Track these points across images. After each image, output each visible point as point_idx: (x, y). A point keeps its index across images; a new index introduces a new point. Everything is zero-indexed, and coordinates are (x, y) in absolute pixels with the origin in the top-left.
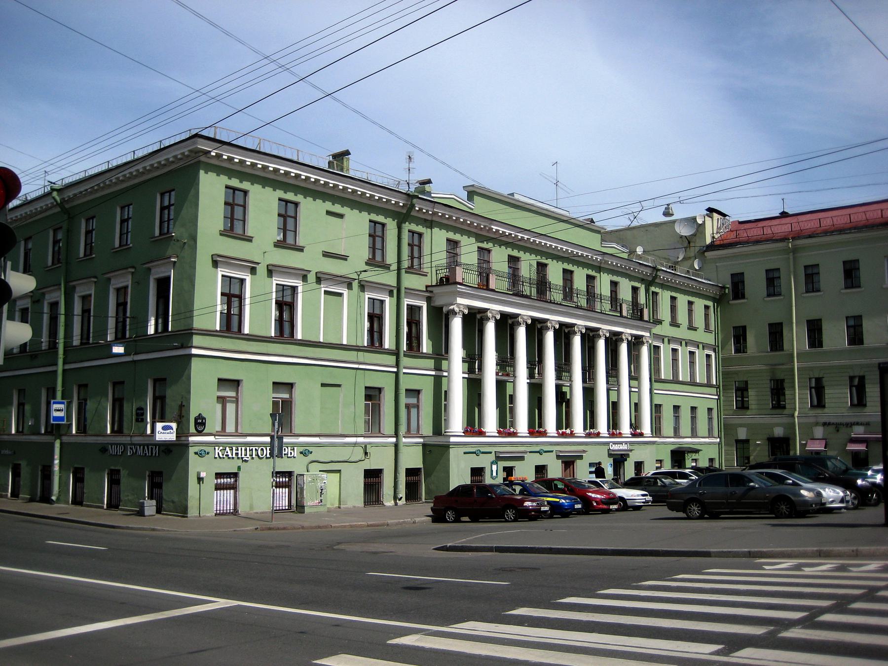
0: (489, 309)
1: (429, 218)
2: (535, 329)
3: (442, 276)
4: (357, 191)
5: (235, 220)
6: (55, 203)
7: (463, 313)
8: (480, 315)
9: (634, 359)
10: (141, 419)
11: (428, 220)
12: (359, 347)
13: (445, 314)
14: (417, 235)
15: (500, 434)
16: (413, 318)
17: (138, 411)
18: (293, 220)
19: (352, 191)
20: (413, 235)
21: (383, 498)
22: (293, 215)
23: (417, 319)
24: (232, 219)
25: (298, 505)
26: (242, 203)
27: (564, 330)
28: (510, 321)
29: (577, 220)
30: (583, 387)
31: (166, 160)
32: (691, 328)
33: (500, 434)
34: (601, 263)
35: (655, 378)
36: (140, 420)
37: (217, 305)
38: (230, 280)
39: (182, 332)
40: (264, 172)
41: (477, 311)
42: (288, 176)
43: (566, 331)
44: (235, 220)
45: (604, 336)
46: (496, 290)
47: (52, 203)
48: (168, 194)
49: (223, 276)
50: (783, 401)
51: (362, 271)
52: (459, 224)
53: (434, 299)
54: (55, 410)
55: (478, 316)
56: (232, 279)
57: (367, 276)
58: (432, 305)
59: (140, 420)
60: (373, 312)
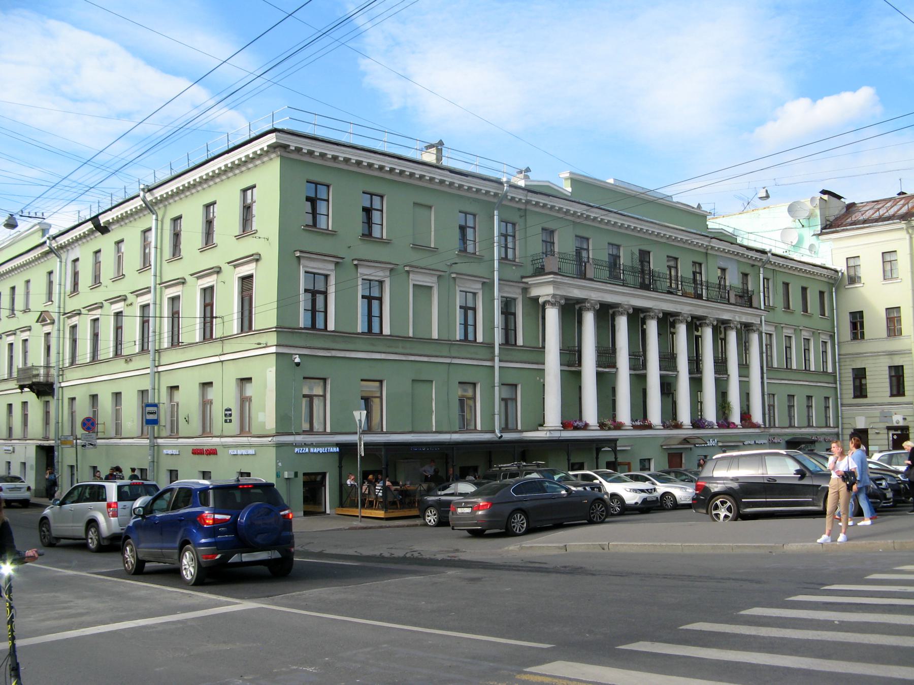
0: (587, 299)
1: (523, 207)
2: (667, 323)
3: (537, 267)
4: (472, 187)
5: (311, 212)
6: (144, 205)
7: (628, 312)
8: (579, 306)
9: (695, 343)
10: (229, 420)
11: (521, 209)
12: (450, 341)
13: (611, 314)
14: (511, 225)
15: (665, 426)
16: (509, 311)
17: (226, 412)
18: (472, 230)
19: (295, 149)
20: (507, 226)
21: (390, 512)
22: (379, 208)
23: (513, 311)
24: (506, 248)
25: (887, 449)
26: (326, 198)
27: (696, 323)
28: (642, 316)
29: (647, 195)
30: (689, 378)
31: (245, 156)
32: (769, 308)
33: (665, 426)
34: (707, 249)
35: (767, 368)
36: (228, 421)
37: (305, 300)
38: (314, 276)
39: (343, 335)
40: (347, 165)
41: (575, 302)
42: (383, 171)
43: (671, 320)
44: (311, 212)
45: (711, 325)
46: (595, 279)
47: (141, 206)
48: (250, 191)
49: (414, 285)
50: (63, 379)
51: (453, 264)
52: (570, 215)
53: (530, 290)
54: (148, 413)
55: (577, 307)
56: (316, 275)
57: (459, 268)
58: (528, 296)
59: (228, 421)
60: (314, 288)
